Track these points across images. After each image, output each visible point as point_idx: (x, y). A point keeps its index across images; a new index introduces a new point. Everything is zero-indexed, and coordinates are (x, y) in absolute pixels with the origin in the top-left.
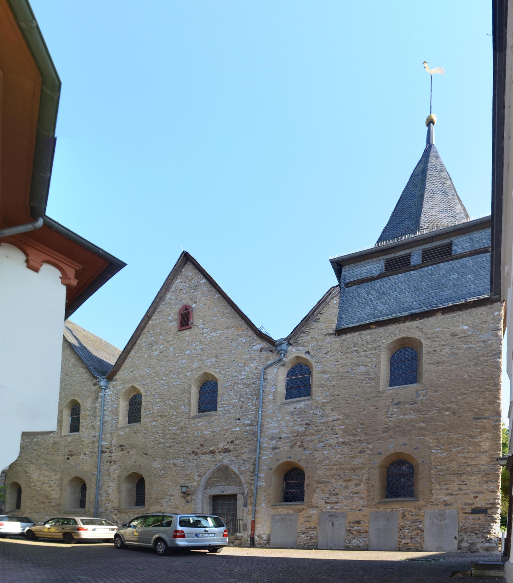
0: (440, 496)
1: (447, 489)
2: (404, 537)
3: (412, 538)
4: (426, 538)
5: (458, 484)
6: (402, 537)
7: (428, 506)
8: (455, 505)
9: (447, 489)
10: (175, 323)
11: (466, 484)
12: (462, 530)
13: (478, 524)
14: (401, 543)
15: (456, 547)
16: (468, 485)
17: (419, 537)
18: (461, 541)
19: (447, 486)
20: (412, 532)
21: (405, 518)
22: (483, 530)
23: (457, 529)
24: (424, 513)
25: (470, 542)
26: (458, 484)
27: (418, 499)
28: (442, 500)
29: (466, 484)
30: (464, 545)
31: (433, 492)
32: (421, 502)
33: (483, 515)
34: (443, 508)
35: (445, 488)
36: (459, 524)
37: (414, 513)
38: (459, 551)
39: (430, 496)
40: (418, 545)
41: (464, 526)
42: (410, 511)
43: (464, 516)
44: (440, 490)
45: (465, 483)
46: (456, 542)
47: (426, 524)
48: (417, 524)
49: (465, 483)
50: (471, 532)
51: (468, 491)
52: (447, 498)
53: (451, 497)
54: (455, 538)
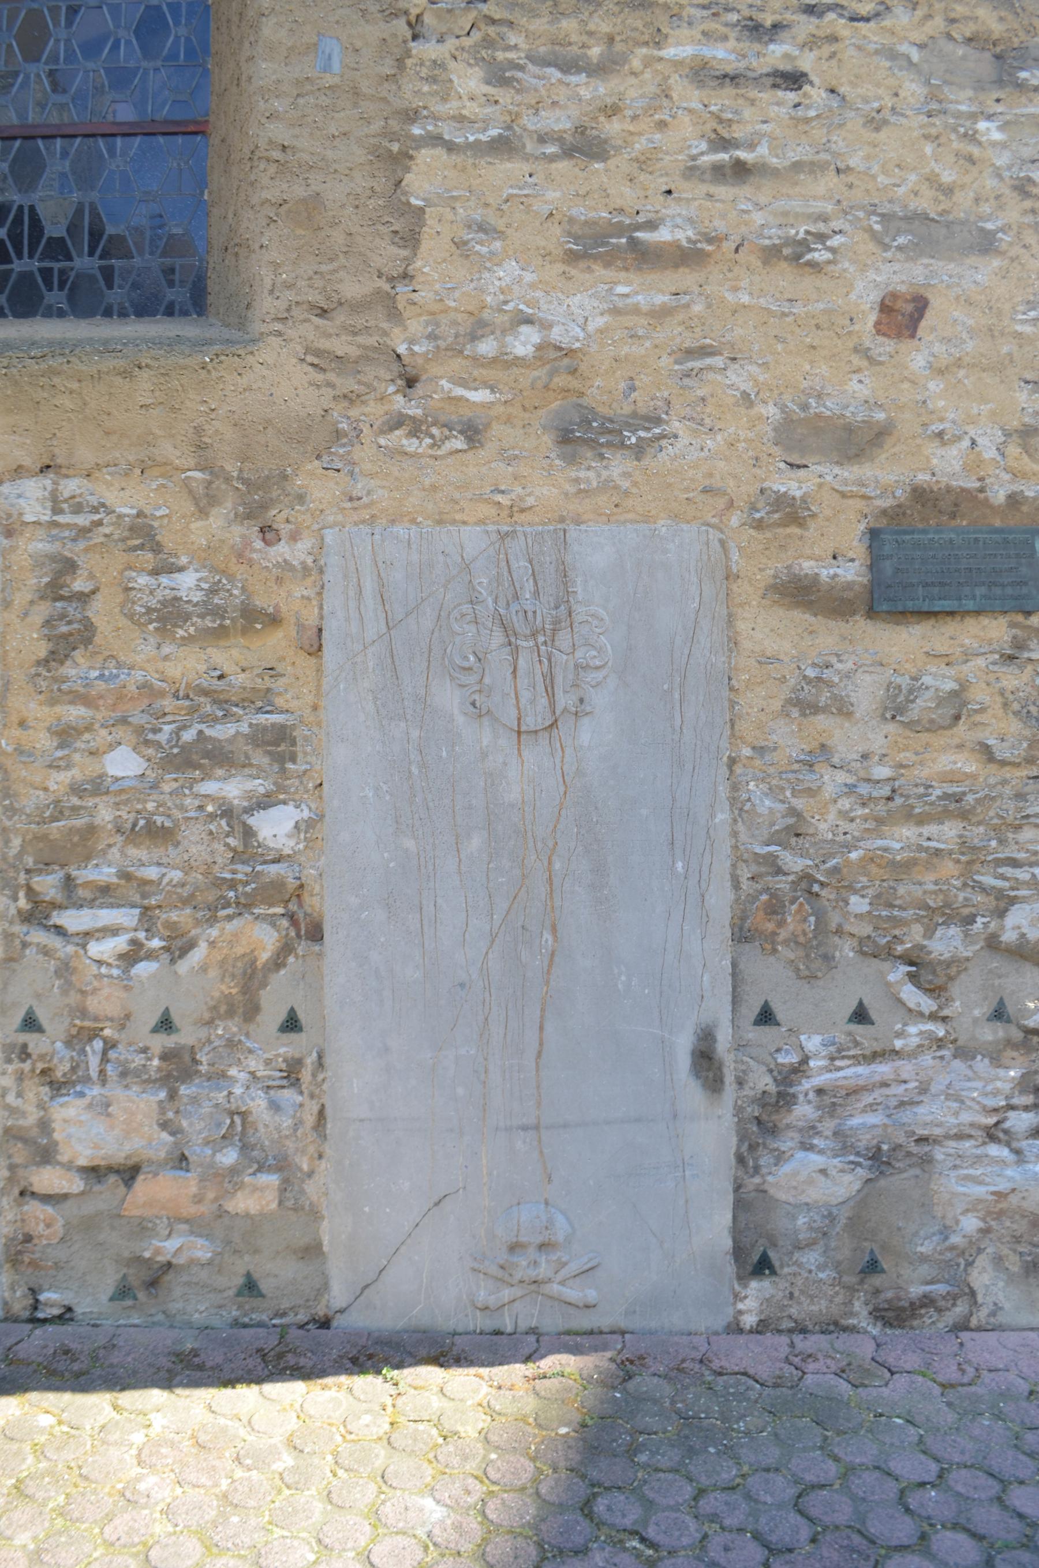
0: (508, 278)
1: (584, 146)
2: (79, 1038)
3: (179, 1067)
4: (355, 1082)
5: (701, 73)
6: (51, 1045)
7: (364, 454)
8: (685, 449)
9: (584, 146)
10: (15, 121)
11: (794, 80)
12: (775, 908)
13: (953, 806)
14: (46, 1155)
15: (716, 1227)
16: (816, 94)
17: (266, 1049)
18: (761, 1127)
19: (589, 89)
20: (179, 947)
21: (79, 669)
22: (1003, 903)
23: (721, 902)
24: (313, 570)
25: (865, 1122)
26: (701, 73)
27: (242, 324)
28: (524, 343)
29: (794, 80)
30: (811, 1179)
31: (427, 177)
32: (274, 376)
33: (997, 630)
34: (547, 484)
35: (559, 121)
36: (739, 807)
37: (188, 583)
38: (753, 1300)
39: (387, 254)
40: (257, 1197)
41: (795, 832)
42: (142, 534)
43: (775, 634)
44: (503, 146)
45: (777, 53)
46: (711, 1131)
47: (343, 819)
48: (233, 789)
49: (777, 53)
50: (873, 951)
51: (819, 194)
52: (579, 309)
53: (631, 288)
54: (705, 1059)
